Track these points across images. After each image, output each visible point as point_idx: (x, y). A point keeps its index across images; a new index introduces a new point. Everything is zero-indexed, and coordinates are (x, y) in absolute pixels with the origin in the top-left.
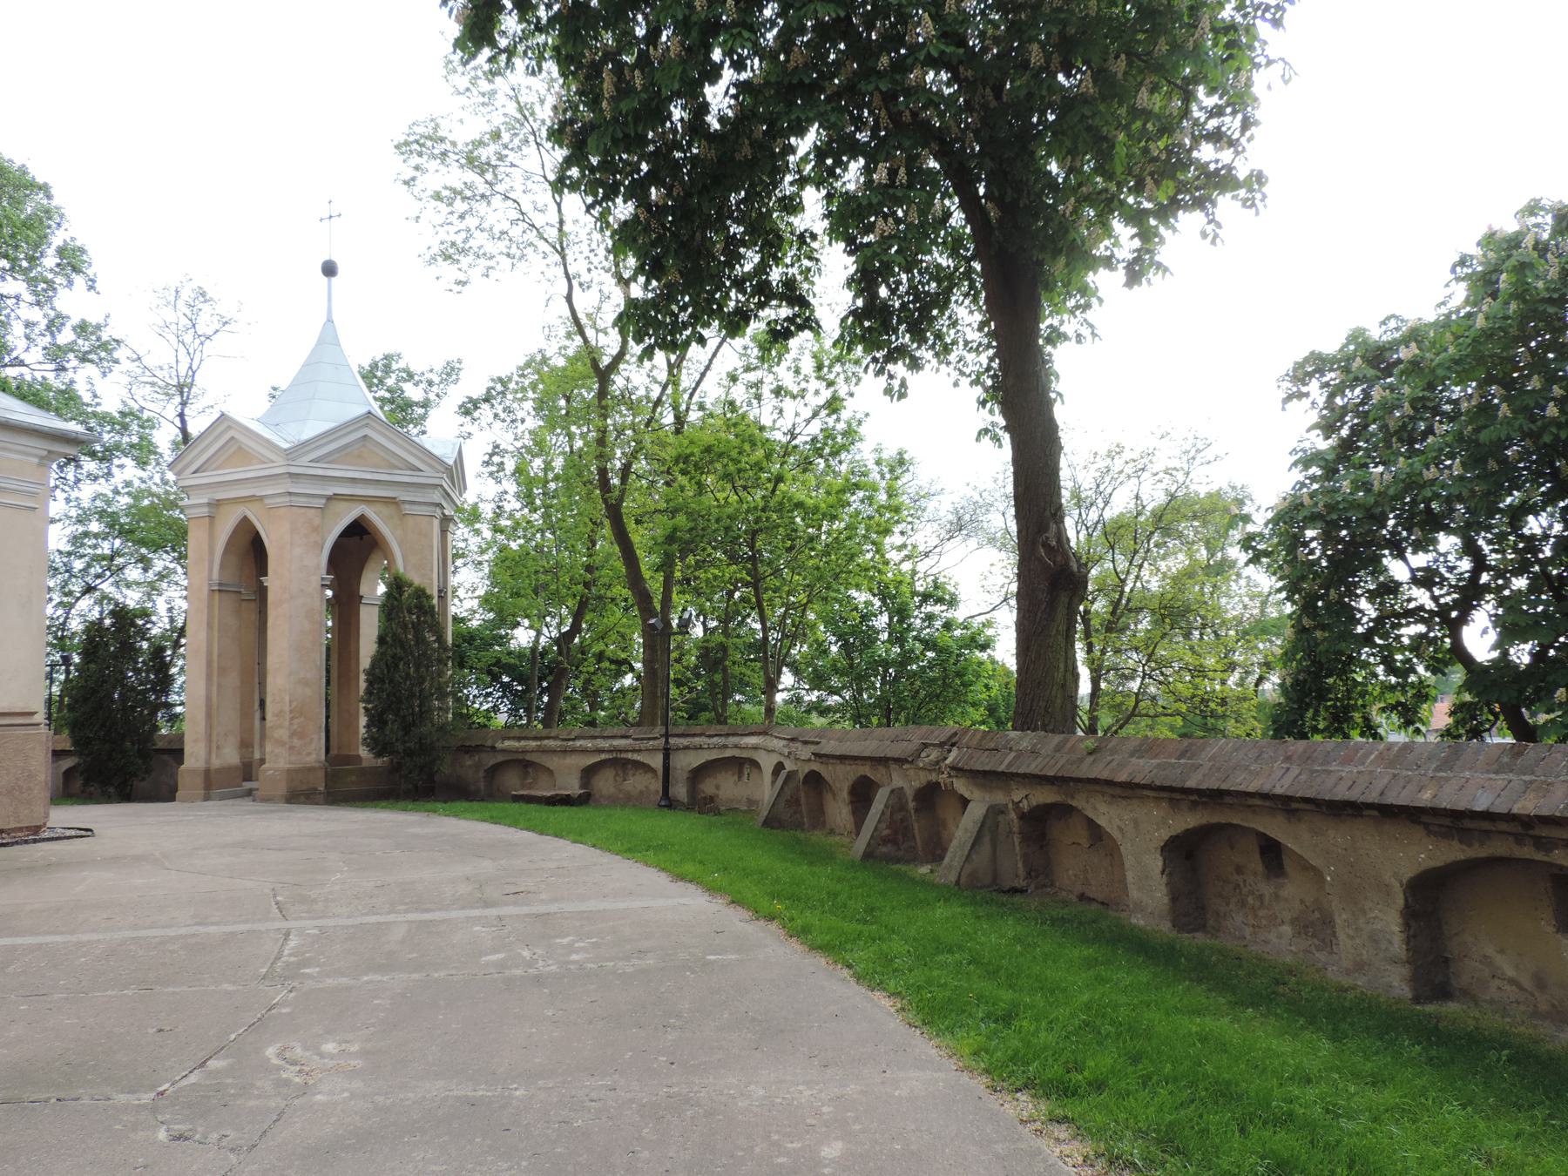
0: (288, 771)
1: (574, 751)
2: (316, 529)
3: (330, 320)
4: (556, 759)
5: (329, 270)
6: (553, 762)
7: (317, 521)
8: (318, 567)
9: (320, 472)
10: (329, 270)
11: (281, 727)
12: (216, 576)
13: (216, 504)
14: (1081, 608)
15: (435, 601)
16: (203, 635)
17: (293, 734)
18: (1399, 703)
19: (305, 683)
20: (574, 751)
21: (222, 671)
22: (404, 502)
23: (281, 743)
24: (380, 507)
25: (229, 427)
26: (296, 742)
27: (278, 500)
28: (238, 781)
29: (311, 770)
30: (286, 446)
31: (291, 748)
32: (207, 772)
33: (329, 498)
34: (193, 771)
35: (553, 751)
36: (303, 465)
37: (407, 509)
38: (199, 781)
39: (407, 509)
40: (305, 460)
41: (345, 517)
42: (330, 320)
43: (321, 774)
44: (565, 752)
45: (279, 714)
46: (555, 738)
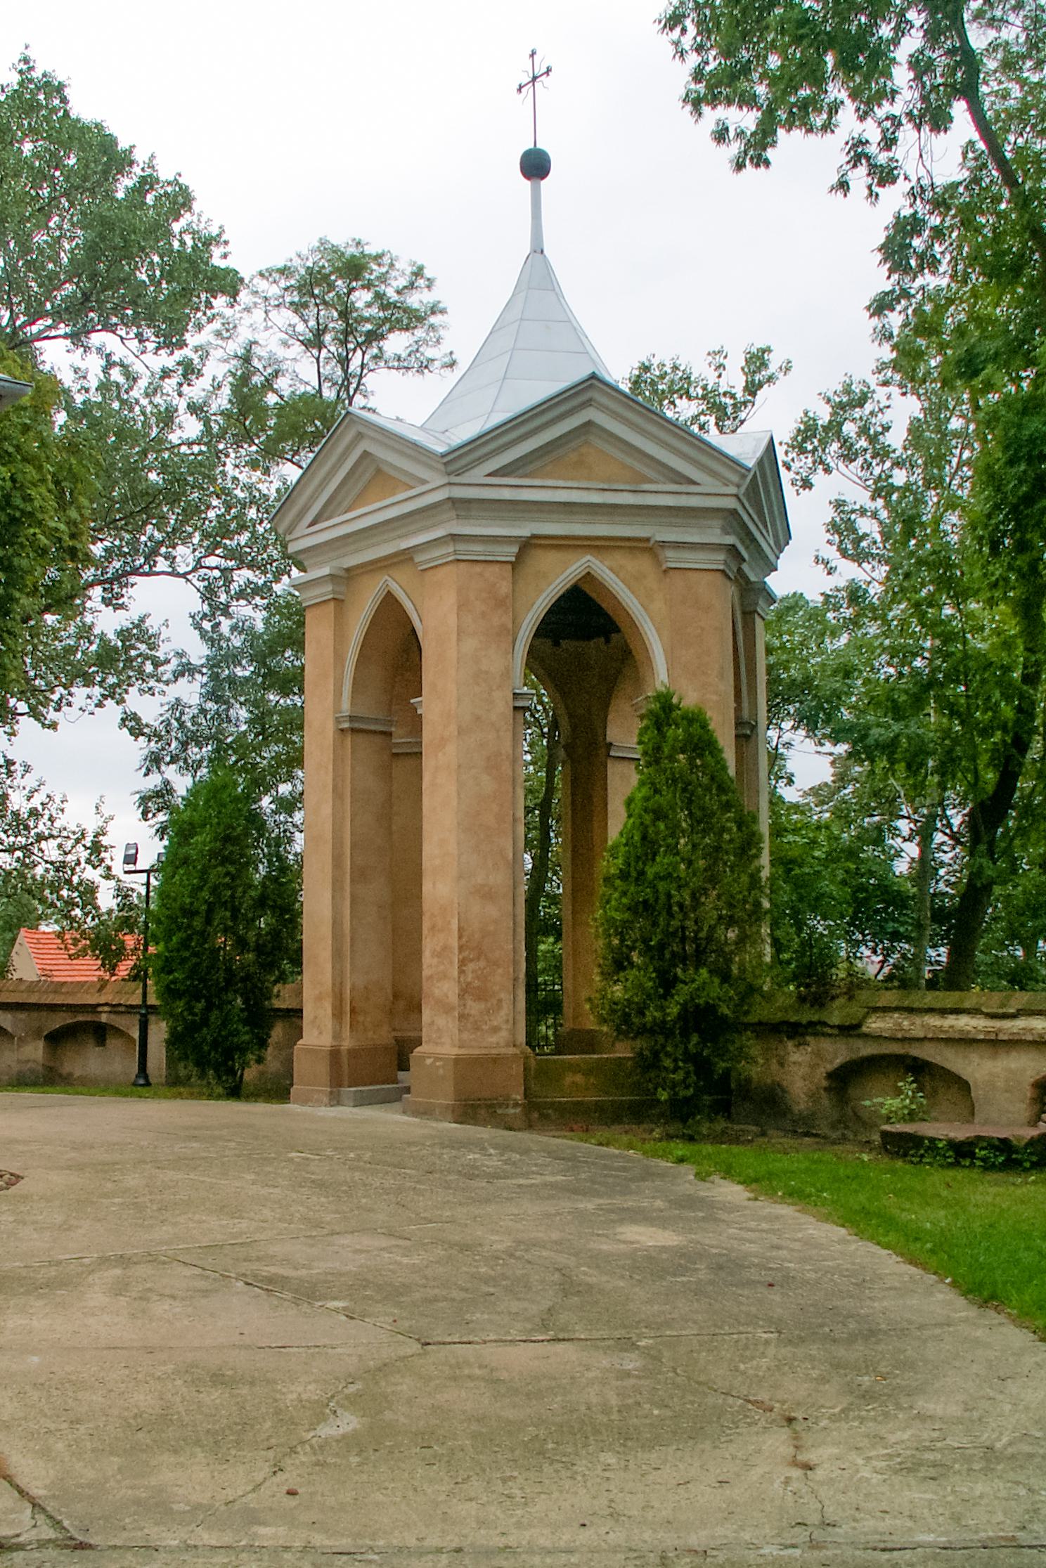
0: (458, 1061)
1: (1014, 1043)
2: (500, 603)
3: (538, 249)
4: (975, 1057)
5: (535, 166)
6: (977, 1069)
7: (504, 587)
8: (507, 673)
9: (507, 494)
10: (535, 166)
11: (444, 976)
12: (346, 706)
13: (349, 577)
14: (976, 445)
15: (729, 756)
16: (327, 810)
17: (464, 992)
18: (717, 424)
19: (487, 894)
20: (1014, 1043)
21: (360, 875)
22: (663, 544)
23: (448, 1009)
24: (619, 558)
25: (360, 436)
26: (474, 1008)
27: (437, 553)
28: (382, 1065)
29: (496, 1060)
30: (441, 449)
31: (462, 1017)
32: (335, 1054)
33: (528, 545)
34: (312, 1051)
35: (966, 1042)
36: (478, 483)
37: (672, 558)
38: (323, 1069)
39: (672, 558)
40: (478, 474)
41: (553, 579)
42: (538, 249)
43: (517, 1069)
44: (995, 1044)
45: (442, 953)
46: (974, 1012)
